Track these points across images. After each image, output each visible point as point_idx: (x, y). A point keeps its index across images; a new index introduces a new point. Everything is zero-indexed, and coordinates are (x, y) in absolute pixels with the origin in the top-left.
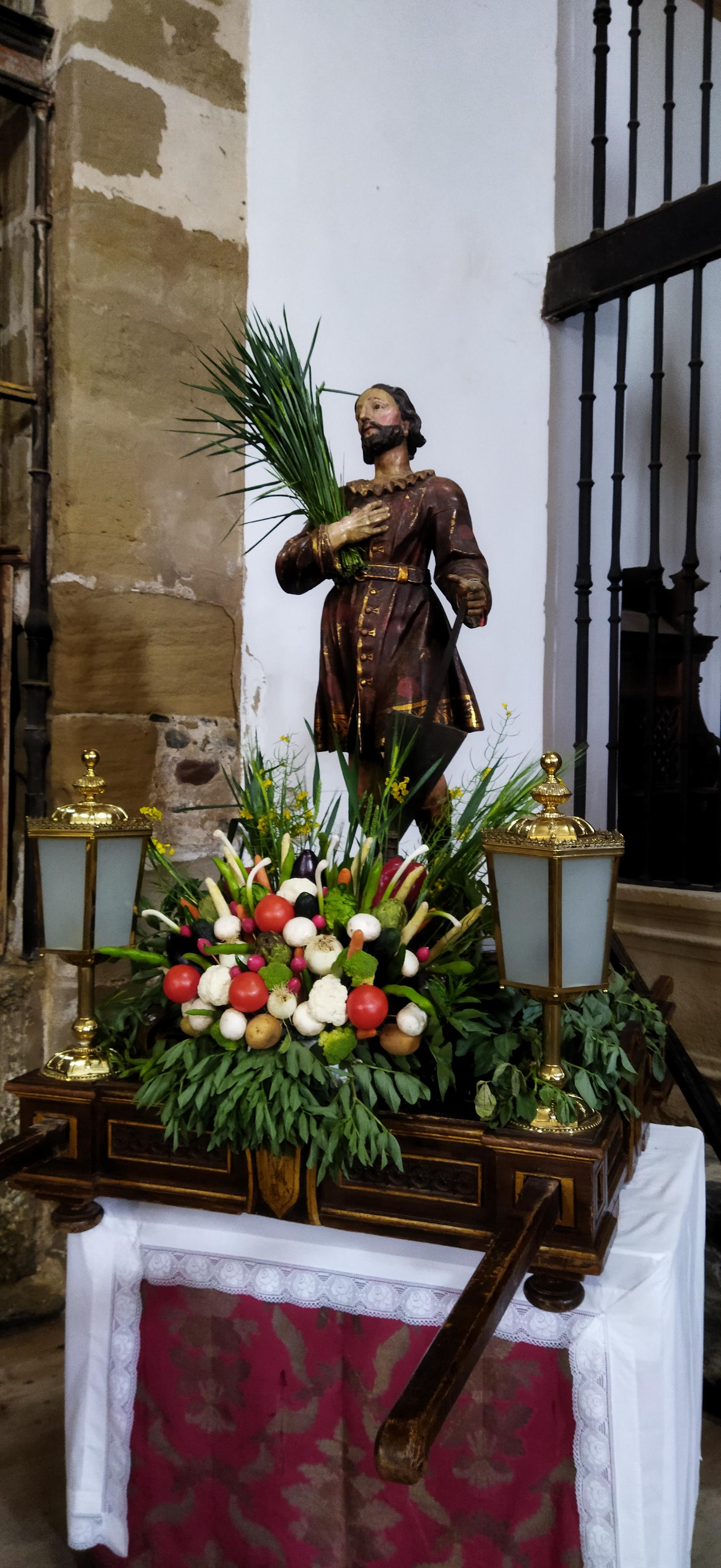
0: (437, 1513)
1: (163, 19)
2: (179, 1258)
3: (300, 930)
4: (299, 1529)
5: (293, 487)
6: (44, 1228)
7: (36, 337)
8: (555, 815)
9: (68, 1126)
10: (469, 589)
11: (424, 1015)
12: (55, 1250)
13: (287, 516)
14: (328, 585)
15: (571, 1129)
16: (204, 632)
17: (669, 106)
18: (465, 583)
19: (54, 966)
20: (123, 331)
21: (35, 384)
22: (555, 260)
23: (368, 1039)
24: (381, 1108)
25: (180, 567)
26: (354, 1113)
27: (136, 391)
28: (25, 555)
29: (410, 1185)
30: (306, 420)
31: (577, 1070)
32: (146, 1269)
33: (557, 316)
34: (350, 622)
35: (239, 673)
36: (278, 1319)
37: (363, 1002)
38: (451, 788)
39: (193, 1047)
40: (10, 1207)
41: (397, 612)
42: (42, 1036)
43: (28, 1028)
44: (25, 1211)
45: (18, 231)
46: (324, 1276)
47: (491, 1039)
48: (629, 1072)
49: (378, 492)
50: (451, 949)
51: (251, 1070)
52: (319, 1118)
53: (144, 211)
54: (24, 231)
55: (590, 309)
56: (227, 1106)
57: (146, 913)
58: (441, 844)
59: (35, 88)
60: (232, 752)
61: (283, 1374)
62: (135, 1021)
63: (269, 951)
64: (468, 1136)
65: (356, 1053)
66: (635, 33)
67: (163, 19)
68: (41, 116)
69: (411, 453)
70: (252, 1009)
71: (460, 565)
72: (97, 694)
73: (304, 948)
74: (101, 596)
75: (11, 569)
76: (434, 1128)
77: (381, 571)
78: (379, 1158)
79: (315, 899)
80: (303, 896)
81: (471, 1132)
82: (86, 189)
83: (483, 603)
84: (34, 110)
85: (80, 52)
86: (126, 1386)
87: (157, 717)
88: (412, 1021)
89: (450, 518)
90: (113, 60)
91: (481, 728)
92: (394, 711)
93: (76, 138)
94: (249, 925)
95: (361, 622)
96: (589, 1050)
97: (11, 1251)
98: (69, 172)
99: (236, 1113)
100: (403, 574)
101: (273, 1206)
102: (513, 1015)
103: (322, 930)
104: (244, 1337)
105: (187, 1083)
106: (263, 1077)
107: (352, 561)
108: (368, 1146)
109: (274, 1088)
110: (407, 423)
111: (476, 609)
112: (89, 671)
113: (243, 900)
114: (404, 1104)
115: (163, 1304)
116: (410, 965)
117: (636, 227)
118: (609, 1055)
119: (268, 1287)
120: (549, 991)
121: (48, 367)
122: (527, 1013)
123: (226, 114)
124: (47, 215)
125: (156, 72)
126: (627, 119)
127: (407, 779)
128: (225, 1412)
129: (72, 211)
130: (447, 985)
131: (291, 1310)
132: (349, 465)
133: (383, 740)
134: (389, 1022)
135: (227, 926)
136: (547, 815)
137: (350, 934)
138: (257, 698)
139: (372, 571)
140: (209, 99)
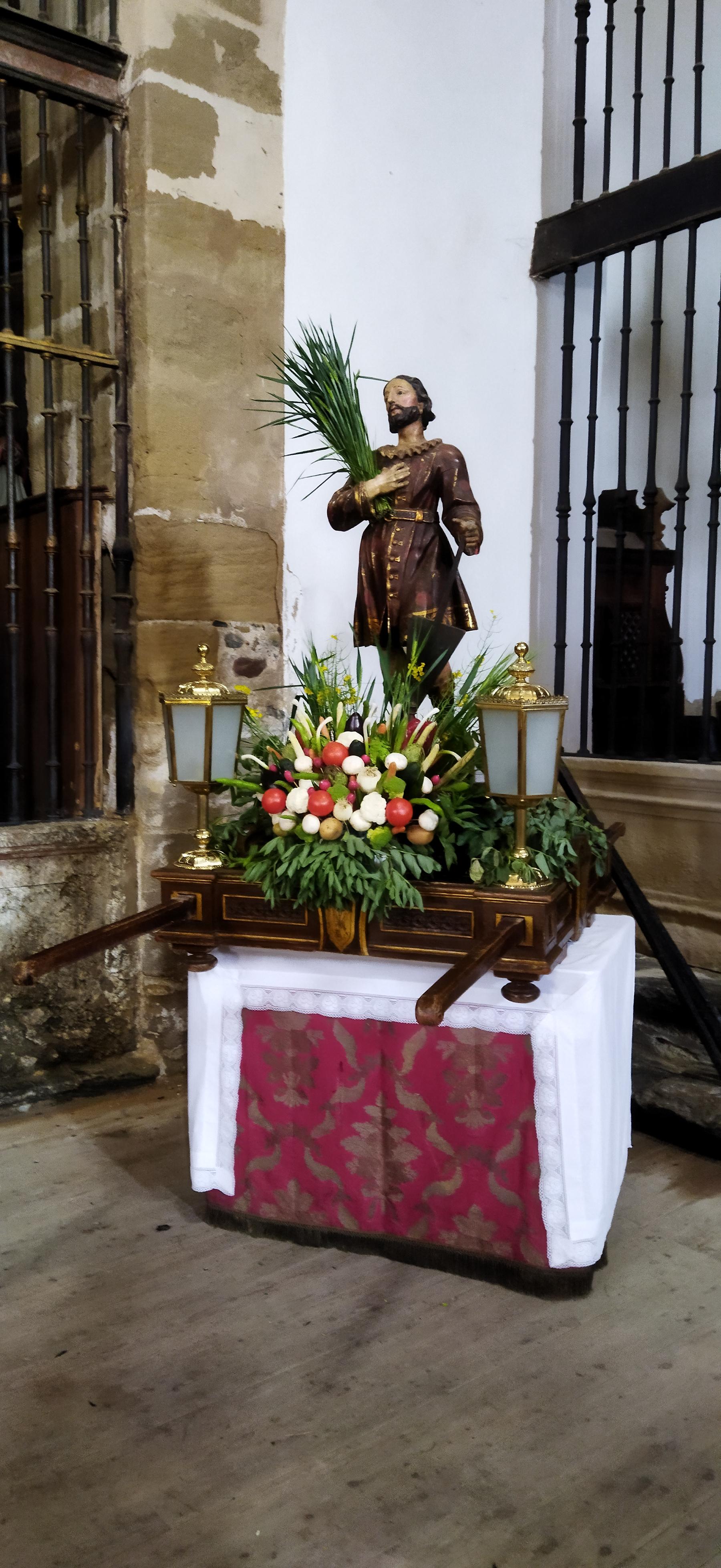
0: (444, 1147)
1: (215, 41)
2: (268, 992)
3: (353, 764)
4: (352, 1166)
5: (341, 453)
6: (141, 1015)
7: (117, 313)
8: (523, 685)
9: (195, 900)
10: (467, 529)
11: (436, 817)
12: (150, 1032)
13: (334, 473)
14: (365, 524)
15: (533, 886)
16: (254, 554)
17: (638, 96)
18: (464, 524)
19: (144, 818)
20: (188, 308)
21: (117, 353)
22: (543, 226)
23: (400, 834)
24: (409, 875)
25: (235, 501)
26: (392, 876)
27: (198, 357)
28: (112, 492)
29: (427, 927)
30: (348, 403)
31: (537, 853)
32: (245, 1001)
33: (542, 275)
34: (381, 552)
35: (281, 587)
36: (337, 1029)
37: (396, 808)
38: (454, 671)
39: (283, 841)
40: (116, 1000)
41: (415, 544)
42: (136, 871)
43: (125, 865)
44: (128, 1002)
45: (97, 222)
46: (368, 998)
47: (479, 833)
48: (572, 856)
49: (401, 456)
50: (454, 778)
51: (324, 852)
52: (370, 880)
53: (201, 206)
54: (103, 222)
55: (571, 271)
56: (309, 874)
57: (244, 757)
58: (447, 709)
59: (113, 104)
60: (276, 651)
61: (341, 1064)
62: (236, 833)
63: (334, 777)
64: (466, 893)
65: (391, 843)
66: (610, 28)
67: (215, 41)
68: (117, 126)
69: (424, 426)
70: (325, 814)
71: (461, 510)
72: (172, 605)
73: (355, 776)
74: (174, 526)
75: (100, 503)
76: (443, 889)
77: (405, 514)
78: (408, 903)
79: (363, 745)
80: (355, 742)
81: (467, 891)
82: (157, 191)
83: (477, 538)
84: (111, 121)
85: (150, 76)
86: (233, 1079)
87: (218, 623)
88: (428, 821)
89: (454, 475)
90: (175, 80)
91: (476, 628)
92: (414, 616)
93: (148, 150)
94: (319, 762)
95: (389, 552)
96: (546, 842)
97: (118, 1032)
98: (144, 177)
99: (315, 880)
100: (419, 516)
101: (337, 945)
102: (496, 820)
103: (368, 764)
104: (313, 1041)
105: (280, 863)
106: (332, 856)
107: (383, 507)
108: (401, 896)
109: (339, 863)
110: (422, 404)
111: (472, 542)
112: (166, 586)
113: (313, 746)
114: (423, 873)
115: (259, 1026)
116: (427, 786)
117: (608, 200)
118: (559, 845)
119: (330, 1008)
120: (517, 798)
121: (127, 338)
122: (505, 820)
123: (266, 118)
124: (124, 210)
125: (210, 88)
126: (603, 105)
127: (423, 664)
128: (300, 1091)
129: (147, 211)
130: (452, 798)
131: (346, 1022)
132: (379, 434)
133: (406, 637)
134: (414, 823)
135: (303, 763)
136: (519, 684)
137: (387, 766)
138: (296, 607)
139: (398, 514)
140: (252, 106)
